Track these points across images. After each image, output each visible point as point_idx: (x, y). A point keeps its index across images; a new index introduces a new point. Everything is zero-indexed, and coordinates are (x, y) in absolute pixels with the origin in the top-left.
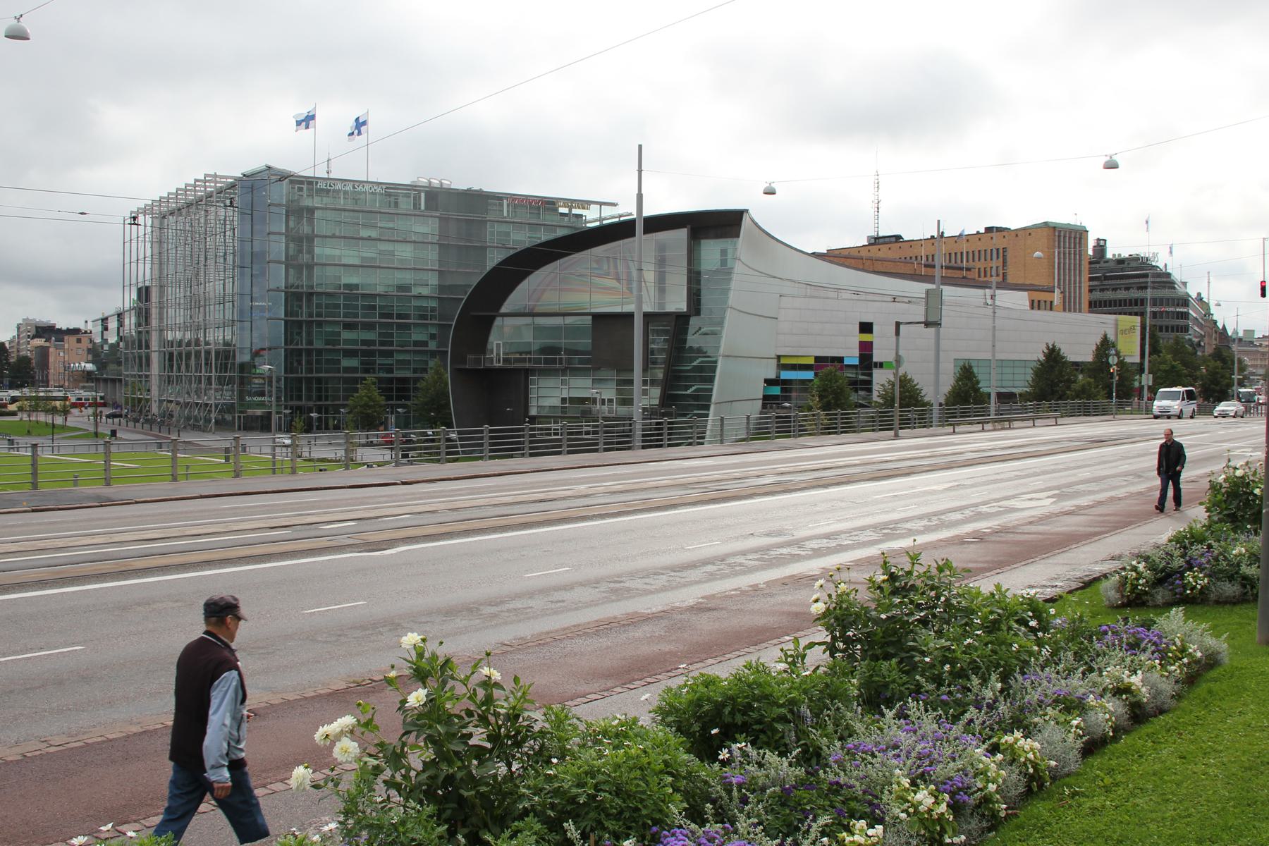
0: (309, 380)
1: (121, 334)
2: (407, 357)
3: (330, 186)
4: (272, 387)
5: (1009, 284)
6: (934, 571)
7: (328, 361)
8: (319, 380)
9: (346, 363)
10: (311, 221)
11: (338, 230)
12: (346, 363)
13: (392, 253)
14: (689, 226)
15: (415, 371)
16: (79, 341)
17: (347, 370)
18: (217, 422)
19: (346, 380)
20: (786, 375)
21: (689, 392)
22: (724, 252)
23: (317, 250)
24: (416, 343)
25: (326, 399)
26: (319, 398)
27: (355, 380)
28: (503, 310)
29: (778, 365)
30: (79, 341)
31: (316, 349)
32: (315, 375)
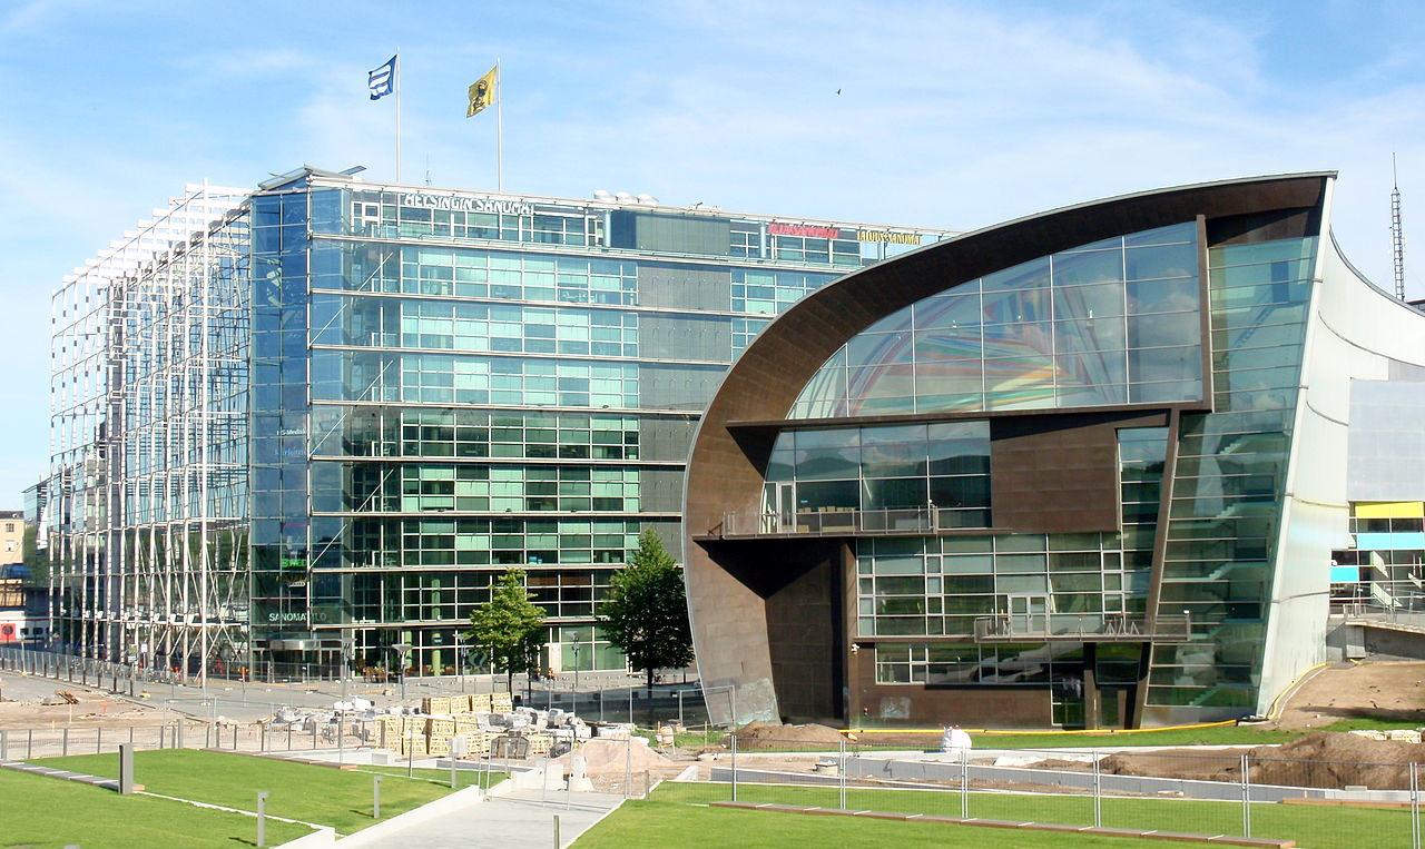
0: (393, 579)
3: (429, 201)
4: (1029, 681)
5: (1167, 457)
7: (428, 541)
8: (412, 578)
9: (464, 543)
10: (392, 378)
11: (445, 290)
12: (464, 543)
14: (1201, 218)
15: (599, 557)
16: (11, 528)
17: (467, 556)
18: (991, 362)
19: (466, 577)
20: (1371, 542)
21: (1213, 578)
22: (1280, 269)
23: (406, 325)
24: (599, 503)
27: (482, 577)
29: (1352, 522)
30: (11, 528)
32: (405, 568)
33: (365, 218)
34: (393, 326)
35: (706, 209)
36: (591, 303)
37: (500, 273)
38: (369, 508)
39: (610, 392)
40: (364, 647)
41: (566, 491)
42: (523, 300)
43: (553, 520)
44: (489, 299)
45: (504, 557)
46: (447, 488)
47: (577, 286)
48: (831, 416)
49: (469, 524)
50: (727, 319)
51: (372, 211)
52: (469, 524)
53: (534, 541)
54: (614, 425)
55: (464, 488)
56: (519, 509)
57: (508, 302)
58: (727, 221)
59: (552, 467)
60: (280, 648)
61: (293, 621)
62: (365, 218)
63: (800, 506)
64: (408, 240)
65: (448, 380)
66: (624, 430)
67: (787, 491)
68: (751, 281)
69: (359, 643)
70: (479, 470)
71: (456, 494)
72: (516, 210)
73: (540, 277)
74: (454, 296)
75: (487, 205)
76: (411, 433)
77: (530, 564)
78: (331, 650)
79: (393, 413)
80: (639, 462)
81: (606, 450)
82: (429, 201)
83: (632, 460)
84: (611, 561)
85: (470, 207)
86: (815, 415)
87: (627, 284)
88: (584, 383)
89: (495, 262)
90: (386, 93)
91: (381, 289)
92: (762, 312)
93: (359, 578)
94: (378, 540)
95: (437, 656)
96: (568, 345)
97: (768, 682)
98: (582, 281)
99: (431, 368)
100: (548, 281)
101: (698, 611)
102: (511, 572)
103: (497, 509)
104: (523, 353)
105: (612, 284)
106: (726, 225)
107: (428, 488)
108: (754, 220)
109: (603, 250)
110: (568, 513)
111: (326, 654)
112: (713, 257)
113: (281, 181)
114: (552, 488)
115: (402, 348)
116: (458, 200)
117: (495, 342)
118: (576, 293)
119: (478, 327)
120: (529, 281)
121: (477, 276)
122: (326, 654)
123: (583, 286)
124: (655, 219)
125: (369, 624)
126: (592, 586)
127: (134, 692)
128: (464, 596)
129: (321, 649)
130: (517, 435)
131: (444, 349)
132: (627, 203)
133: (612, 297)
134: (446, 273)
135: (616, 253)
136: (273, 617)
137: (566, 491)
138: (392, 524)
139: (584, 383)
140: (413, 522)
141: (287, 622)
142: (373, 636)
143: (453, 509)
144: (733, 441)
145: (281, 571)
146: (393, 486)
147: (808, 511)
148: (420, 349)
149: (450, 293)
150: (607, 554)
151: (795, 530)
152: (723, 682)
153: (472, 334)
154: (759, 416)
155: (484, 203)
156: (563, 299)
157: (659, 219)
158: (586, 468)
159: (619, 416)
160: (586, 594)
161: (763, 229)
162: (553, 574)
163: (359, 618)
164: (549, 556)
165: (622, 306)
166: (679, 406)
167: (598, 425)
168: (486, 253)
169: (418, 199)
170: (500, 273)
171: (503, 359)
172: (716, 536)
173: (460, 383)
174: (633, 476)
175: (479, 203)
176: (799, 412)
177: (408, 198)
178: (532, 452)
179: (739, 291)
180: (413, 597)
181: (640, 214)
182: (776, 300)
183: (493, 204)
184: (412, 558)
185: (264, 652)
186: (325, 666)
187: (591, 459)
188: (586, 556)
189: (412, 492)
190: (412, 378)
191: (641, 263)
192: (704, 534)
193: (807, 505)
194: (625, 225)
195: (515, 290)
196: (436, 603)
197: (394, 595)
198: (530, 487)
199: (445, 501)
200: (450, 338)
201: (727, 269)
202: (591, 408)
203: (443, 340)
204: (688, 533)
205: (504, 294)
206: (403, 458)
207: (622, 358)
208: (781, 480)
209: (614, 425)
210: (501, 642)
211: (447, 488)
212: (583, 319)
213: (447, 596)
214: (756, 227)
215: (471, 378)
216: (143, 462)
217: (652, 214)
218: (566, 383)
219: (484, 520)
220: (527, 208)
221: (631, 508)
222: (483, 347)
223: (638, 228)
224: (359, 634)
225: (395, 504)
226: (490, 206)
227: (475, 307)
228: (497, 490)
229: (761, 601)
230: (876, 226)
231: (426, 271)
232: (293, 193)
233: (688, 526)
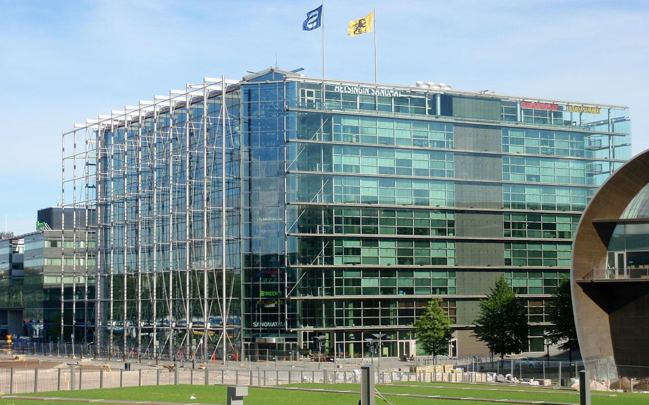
0: (329, 303)
1: (14, 261)
2: (425, 275)
6: (553, 344)
7: (347, 282)
8: (340, 302)
9: (366, 283)
10: (328, 189)
11: (354, 140)
13: (409, 162)
17: (368, 291)
19: (368, 302)
23: (335, 160)
24: (435, 261)
25: (347, 324)
26: (340, 323)
27: (374, 302)
28: (625, 216)
31: (335, 269)
32: (336, 297)
33: (307, 98)
34: (329, 159)
35: (489, 93)
36: (430, 147)
37: (384, 130)
38: (315, 263)
39: (439, 197)
40: (308, 342)
41: (418, 253)
42: (395, 145)
43: (412, 270)
44: (378, 145)
45: (386, 291)
46: (357, 252)
47: (421, 137)
48: (635, 218)
49: (370, 272)
50: (500, 156)
51: (310, 94)
52: (370, 272)
53: (401, 282)
54: (441, 217)
55: (366, 252)
56: (395, 265)
57: (387, 146)
58: (498, 100)
59: (411, 240)
60: (263, 342)
61: (268, 327)
62: (307, 98)
63: (628, 264)
64: (338, 111)
65: (357, 190)
66: (447, 219)
67: (621, 256)
68: (511, 134)
69: (305, 339)
70: (372, 242)
71: (362, 256)
72: (391, 94)
73: (403, 133)
74: (360, 143)
75: (377, 91)
76: (338, 220)
77: (399, 295)
78: (291, 343)
79: (329, 210)
80: (455, 237)
81: (437, 231)
82: (347, 89)
83: (451, 236)
84: (440, 294)
85: (368, 93)
86: (630, 217)
87: (449, 136)
88: (426, 193)
89: (380, 124)
90: (316, 27)
91: (320, 138)
92: (518, 153)
93: (305, 302)
94: (321, 281)
95: (352, 347)
96: (418, 171)
97: (612, 358)
98: (426, 134)
99: (350, 184)
100: (407, 135)
101: (580, 320)
102: (434, 299)
103: (382, 264)
104: (395, 175)
105: (439, 136)
106: (498, 103)
107: (347, 251)
108: (513, 100)
109: (436, 117)
110: (419, 266)
111: (288, 346)
112: (492, 121)
113: (255, 76)
114: (410, 252)
115: (334, 172)
116: (362, 88)
117: (382, 169)
118: (420, 141)
119: (371, 161)
120: (398, 135)
121: (371, 132)
122: (288, 346)
123: (425, 137)
124: (462, 99)
125: (310, 329)
126: (362, 308)
127: (195, 366)
128: (366, 313)
129: (285, 343)
130: (392, 222)
131: (353, 174)
132: (446, 89)
133: (441, 144)
134: (355, 129)
135: (442, 119)
136: (256, 324)
137: (418, 253)
138: (328, 272)
139: (426, 193)
140: (340, 271)
141: (264, 327)
142: (313, 334)
143: (360, 263)
144: (595, 230)
145: (260, 298)
146: (329, 251)
147: (633, 267)
148: (342, 173)
149: (357, 141)
150: (438, 290)
151: (626, 277)
152: (592, 358)
153: (369, 165)
154: (608, 218)
155: (375, 90)
156: (414, 145)
157: (466, 100)
158: (428, 241)
159: (444, 211)
160: (376, 313)
161: (519, 105)
162: (412, 300)
163: (305, 325)
164: (409, 291)
165: (446, 149)
166: (475, 205)
167: (433, 216)
168: (393, 120)
169: (341, 88)
170: (384, 130)
171: (385, 179)
172: (588, 280)
173: (363, 193)
174: (450, 245)
175: (373, 90)
176: (625, 216)
177: (336, 87)
178: (401, 231)
179: (506, 140)
180: (339, 313)
181: (456, 97)
182: (525, 145)
183: (380, 91)
184: (339, 292)
185: (250, 344)
186: (277, 352)
187: (431, 236)
188: (427, 291)
189: (340, 254)
190: (338, 189)
191: (456, 124)
192: (580, 279)
193: (633, 264)
194: (448, 101)
195: (390, 140)
196: (351, 316)
197: (329, 312)
198: (400, 251)
199: (355, 259)
200: (358, 167)
201: (499, 128)
202: (430, 207)
203: (354, 168)
204: (574, 279)
205: (385, 142)
206: (335, 235)
207: (446, 178)
208: (617, 250)
209: (441, 217)
210: (433, 337)
211: (357, 252)
212: (426, 157)
213: (357, 313)
214: (515, 104)
215: (369, 190)
216: (168, 237)
217: (461, 97)
218: (417, 193)
219: (376, 270)
220: (397, 93)
221: (451, 264)
222: (374, 172)
223: (454, 105)
224: (305, 334)
225: (330, 261)
226: (378, 92)
227: (370, 150)
228: (382, 253)
229: (607, 315)
230: (577, 103)
231: (345, 128)
232: (267, 83)
233: (575, 274)
